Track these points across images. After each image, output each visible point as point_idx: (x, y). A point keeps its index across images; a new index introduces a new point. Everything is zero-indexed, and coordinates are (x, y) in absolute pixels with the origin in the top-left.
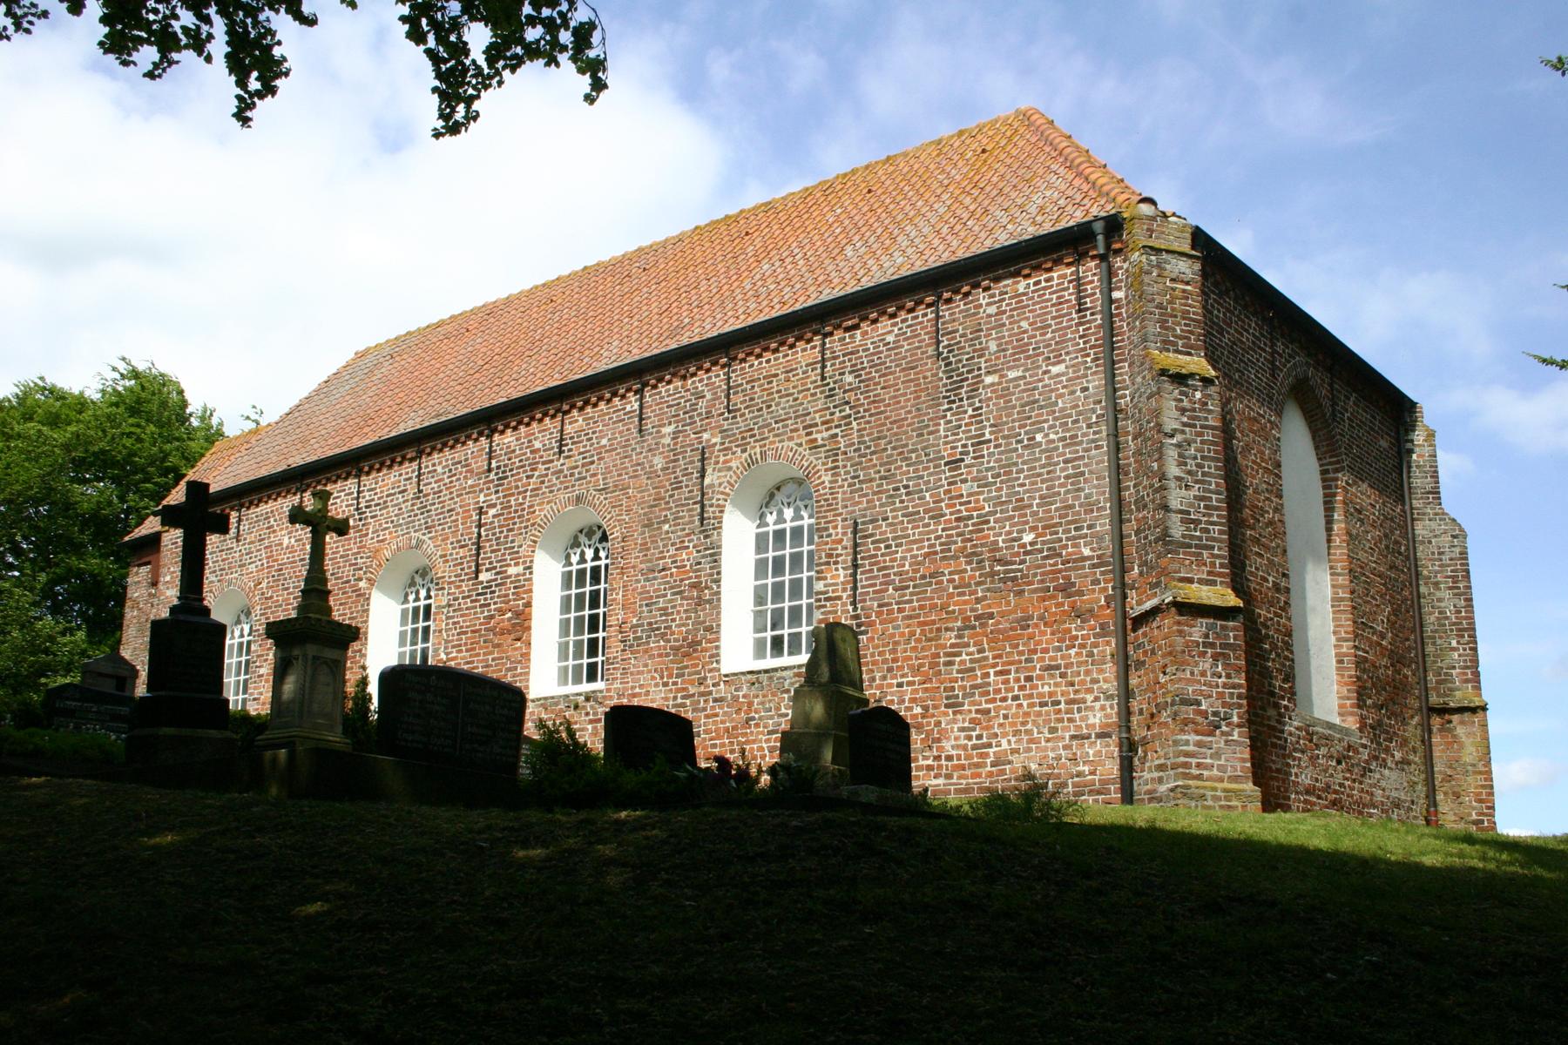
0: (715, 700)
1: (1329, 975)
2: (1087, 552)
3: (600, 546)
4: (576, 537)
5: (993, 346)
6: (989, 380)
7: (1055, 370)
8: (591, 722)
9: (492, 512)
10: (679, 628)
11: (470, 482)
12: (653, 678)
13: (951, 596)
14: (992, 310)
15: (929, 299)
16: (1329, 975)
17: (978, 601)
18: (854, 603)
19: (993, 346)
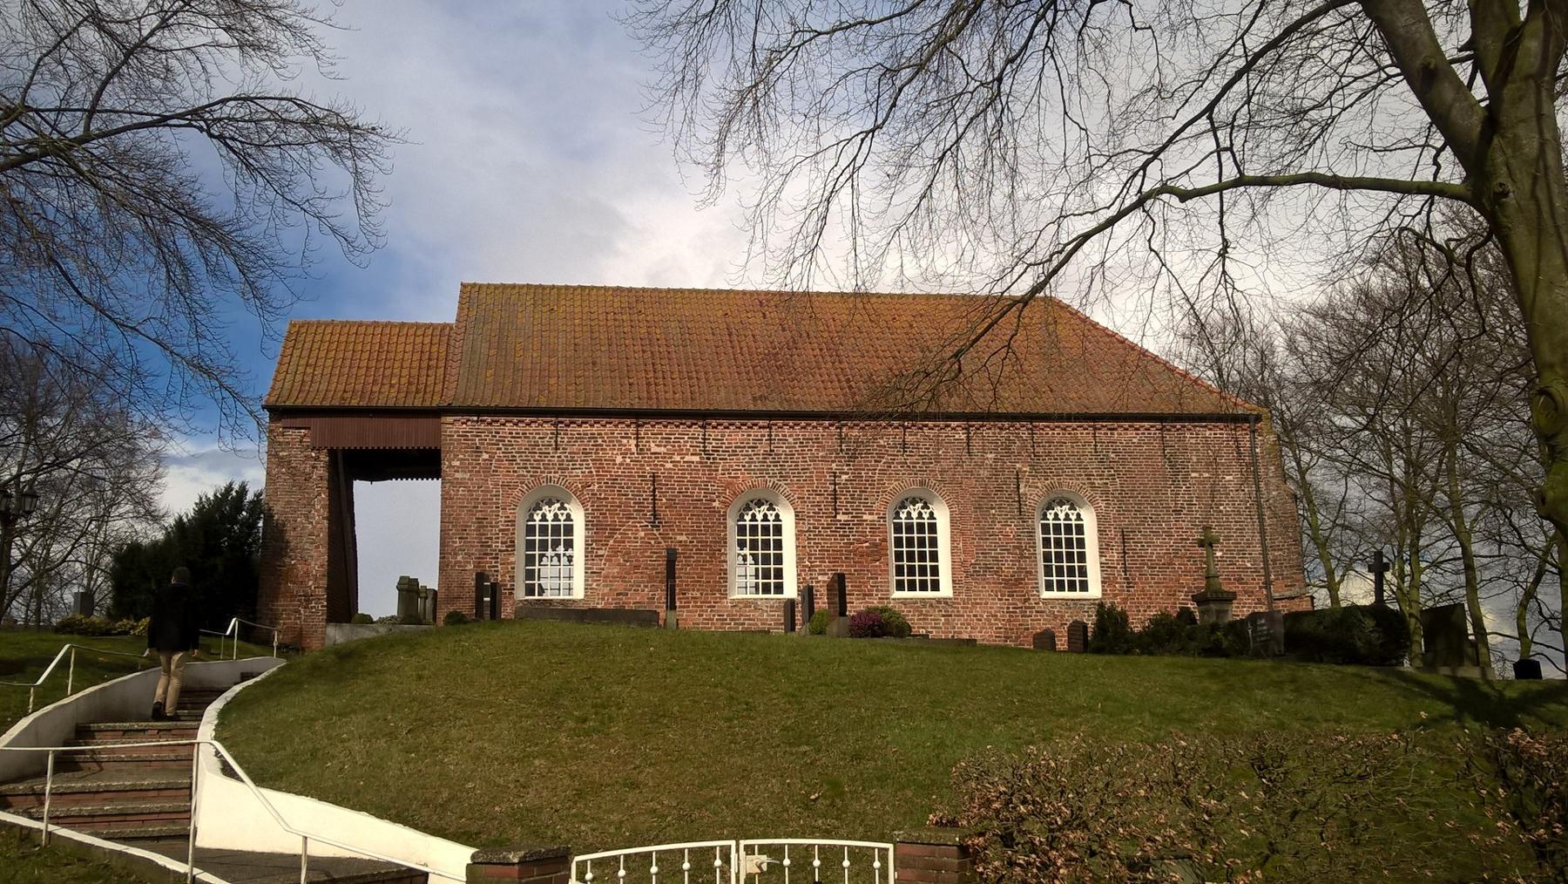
0: (1037, 612)
1: (1243, 794)
2: (1249, 565)
3: (1070, 512)
4: (903, 502)
5: (1195, 459)
6: (1193, 475)
7: (1228, 478)
8: (943, 616)
9: (844, 477)
10: (1008, 567)
11: (821, 454)
12: (990, 595)
13: (1180, 575)
14: (1193, 441)
15: (700, 423)
16: (1243, 794)
17: (1195, 580)
18: (1125, 572)
19: (1195, 459)
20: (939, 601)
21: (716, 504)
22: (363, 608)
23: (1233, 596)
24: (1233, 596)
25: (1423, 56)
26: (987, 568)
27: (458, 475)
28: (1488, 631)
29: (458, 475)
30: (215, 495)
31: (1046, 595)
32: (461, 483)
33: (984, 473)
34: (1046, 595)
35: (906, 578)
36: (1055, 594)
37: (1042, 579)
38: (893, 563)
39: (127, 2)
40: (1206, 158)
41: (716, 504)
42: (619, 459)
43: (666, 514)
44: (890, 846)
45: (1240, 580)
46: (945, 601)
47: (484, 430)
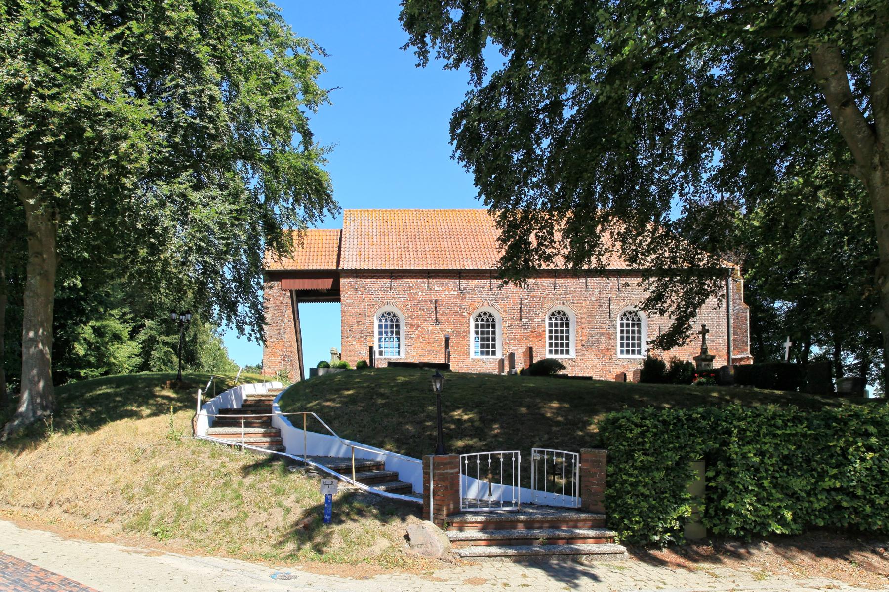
20: (569, 359)
21: (465, 314)
22: (300, 305)
23: (713, 357)
24: (713, 357)
25: (105, 323)
26: (593, 344)
27: (348, 301)
28: (334, 268)
29: (348, 301)
30: (457, 65)
31: (620, 356)
32: (350, 305)
33: (593, 299)
34: (620, 356)
35: (559, 348)
36: (625, 356)
37: (619, 348)
38: (547, 341)
39: (458, 588)
40: (340, 247)
41: (465, 314)
42: (420, 293)
43: (442, 319)
44: (519, 452)
45: (716, 349)
46: (572, 359)
47: (360, 282)
